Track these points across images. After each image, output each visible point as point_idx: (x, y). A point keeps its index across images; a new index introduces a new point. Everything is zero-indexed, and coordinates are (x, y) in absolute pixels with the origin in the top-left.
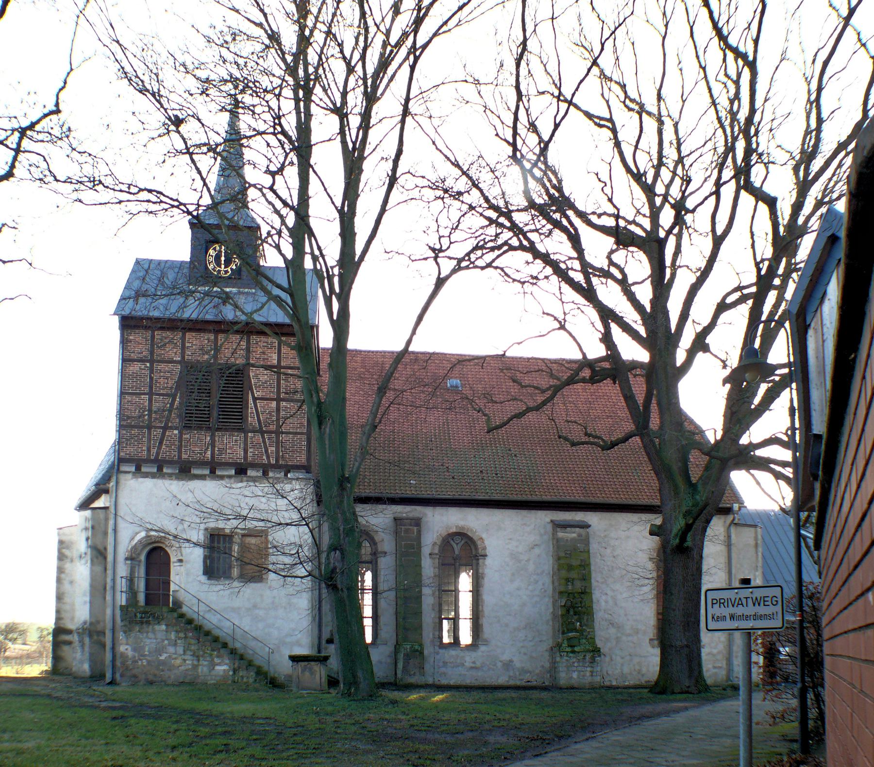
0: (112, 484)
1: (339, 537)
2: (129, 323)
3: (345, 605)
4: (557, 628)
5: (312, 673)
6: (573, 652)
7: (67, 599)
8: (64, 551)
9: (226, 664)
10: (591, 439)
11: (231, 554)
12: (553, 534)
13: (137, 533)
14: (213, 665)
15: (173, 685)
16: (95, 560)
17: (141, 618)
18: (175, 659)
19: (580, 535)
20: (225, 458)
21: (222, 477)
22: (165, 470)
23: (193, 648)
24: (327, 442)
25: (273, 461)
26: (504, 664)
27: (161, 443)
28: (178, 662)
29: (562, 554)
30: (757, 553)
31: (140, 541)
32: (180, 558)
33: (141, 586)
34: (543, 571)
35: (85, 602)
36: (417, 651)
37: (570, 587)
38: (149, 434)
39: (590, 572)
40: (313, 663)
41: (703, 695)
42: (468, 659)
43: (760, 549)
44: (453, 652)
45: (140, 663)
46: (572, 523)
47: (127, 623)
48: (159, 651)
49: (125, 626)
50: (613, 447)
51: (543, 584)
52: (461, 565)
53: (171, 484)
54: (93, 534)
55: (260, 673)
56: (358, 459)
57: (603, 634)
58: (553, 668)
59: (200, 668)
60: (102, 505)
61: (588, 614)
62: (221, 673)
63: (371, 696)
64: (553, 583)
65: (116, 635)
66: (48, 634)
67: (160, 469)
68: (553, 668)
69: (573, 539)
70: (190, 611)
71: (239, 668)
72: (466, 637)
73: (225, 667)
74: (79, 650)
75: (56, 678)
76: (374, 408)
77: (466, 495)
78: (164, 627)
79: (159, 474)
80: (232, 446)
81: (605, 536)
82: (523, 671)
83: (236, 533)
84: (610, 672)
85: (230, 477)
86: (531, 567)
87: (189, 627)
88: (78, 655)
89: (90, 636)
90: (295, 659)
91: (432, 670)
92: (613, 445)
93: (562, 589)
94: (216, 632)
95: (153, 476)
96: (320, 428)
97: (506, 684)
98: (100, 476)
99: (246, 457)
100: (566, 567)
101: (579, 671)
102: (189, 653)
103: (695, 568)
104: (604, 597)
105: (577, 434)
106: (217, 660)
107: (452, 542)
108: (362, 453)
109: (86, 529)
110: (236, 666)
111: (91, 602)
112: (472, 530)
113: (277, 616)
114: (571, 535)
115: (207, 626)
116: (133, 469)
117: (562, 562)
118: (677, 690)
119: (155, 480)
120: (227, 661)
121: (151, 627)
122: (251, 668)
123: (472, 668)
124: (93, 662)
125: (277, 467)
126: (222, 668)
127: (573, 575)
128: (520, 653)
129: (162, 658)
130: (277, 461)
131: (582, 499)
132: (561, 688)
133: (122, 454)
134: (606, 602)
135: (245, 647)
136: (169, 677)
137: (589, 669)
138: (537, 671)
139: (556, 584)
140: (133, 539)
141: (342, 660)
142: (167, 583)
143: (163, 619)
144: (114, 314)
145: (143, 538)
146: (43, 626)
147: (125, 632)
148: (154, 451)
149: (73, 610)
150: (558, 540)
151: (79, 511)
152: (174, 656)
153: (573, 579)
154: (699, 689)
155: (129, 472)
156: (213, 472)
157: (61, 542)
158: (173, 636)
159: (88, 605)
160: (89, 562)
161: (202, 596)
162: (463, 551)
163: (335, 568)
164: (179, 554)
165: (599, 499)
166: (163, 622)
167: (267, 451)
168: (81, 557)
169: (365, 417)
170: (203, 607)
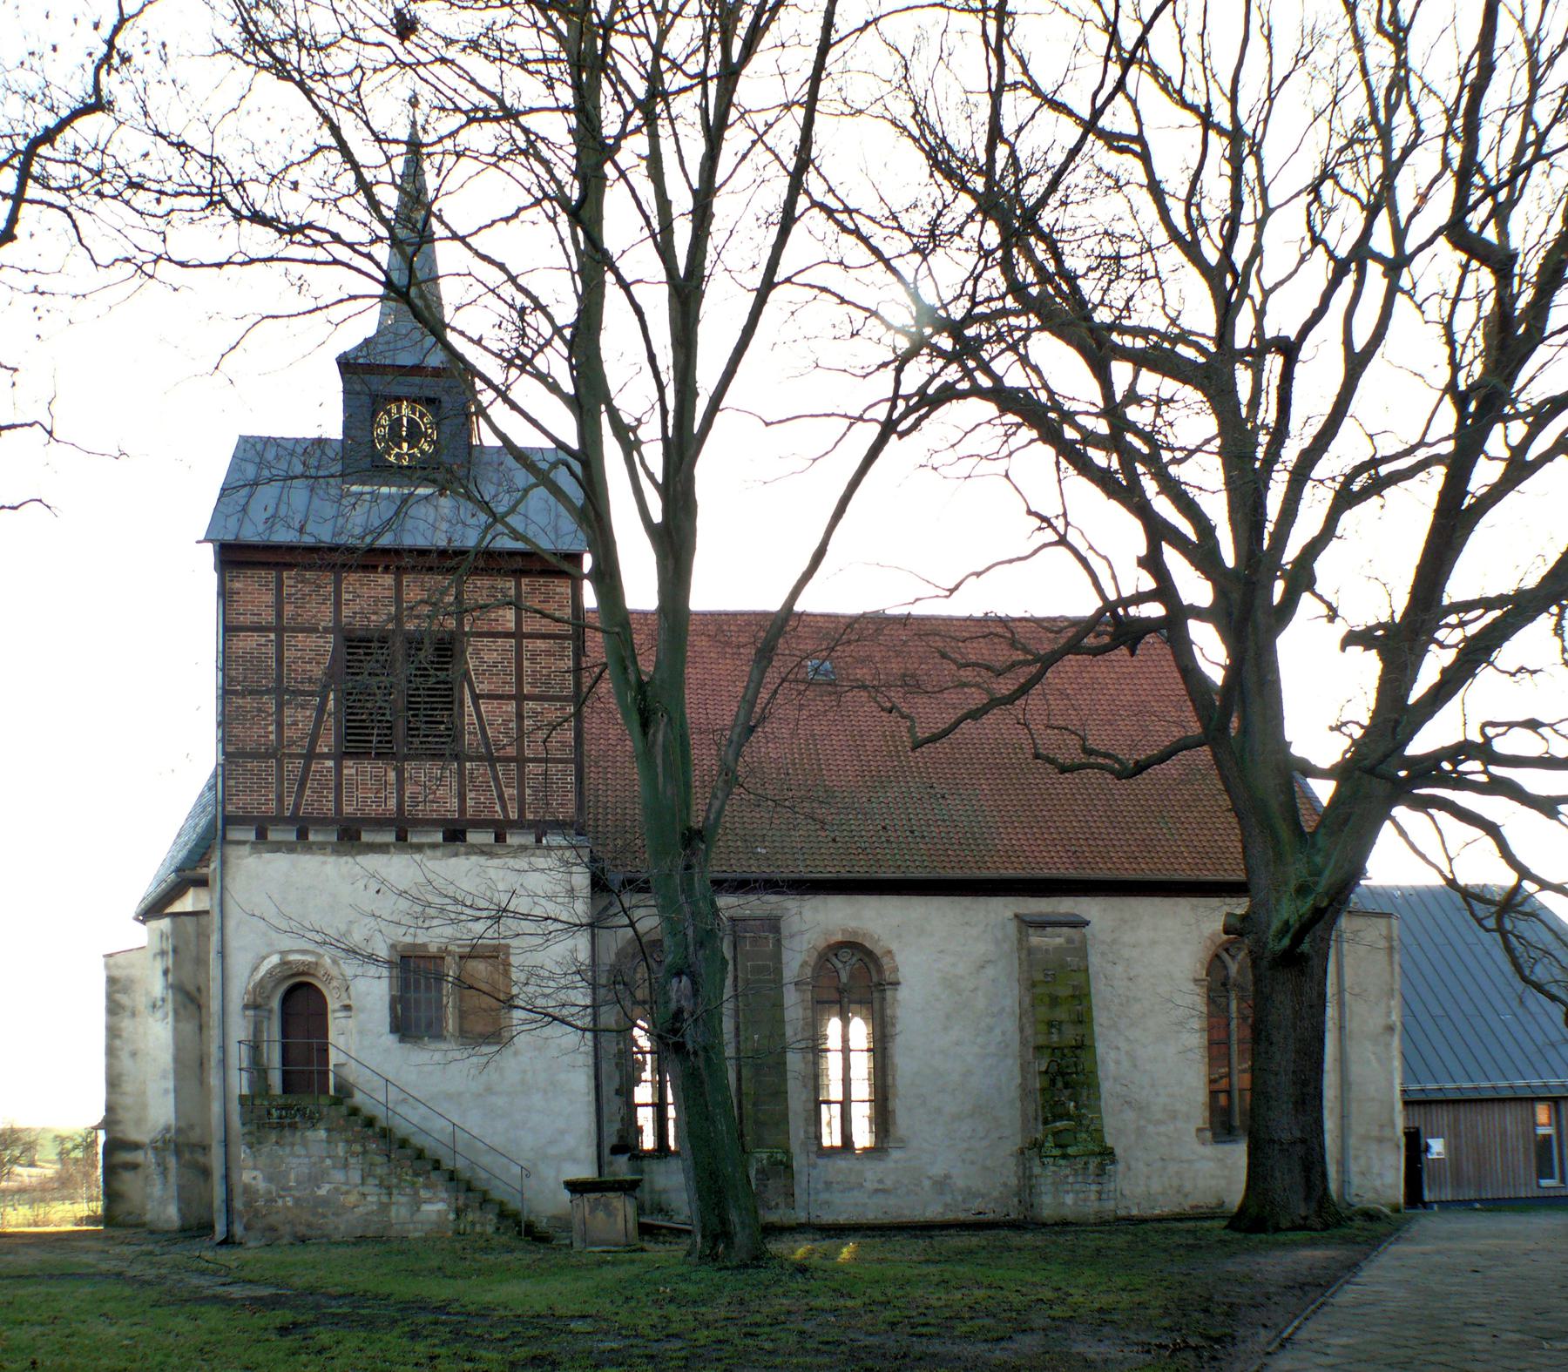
0: (214, 865)
1: (687, 948)
2: (233, 557)
3: (702, 1083)
4: (1031, 1113)
5: (610, 1213)
6: (1065, 1156)
7: (128, 1087)
8: (118, 996)
9: (443, 1200)
10: (1091, 759)
11: (437, 992)
12: (1020, 941)
13: (264, 958)
14: (417, 1203)
15: (346, 1243)
16: (182, 1011)
17: (280, 1117)
18: (347, 1193)
19: (1070, 941)
20: (422, 811)
21: (419, 848)
22: (312, 837)
23: (379, 1171)
24: (659, 761)
25: (513, 815)
26: (936, 1183)
27: (302, 785)
28: (352, 1198)
29: (1039, 976)
30: (1391, 963)
31: (270, 972)
32: (347, 1002)
33: (273, 1056)
34: (1003, 1009)
35: (166, 1091)
36: (781, 1162)
37: (1055, 1038)
38: (280, 767)
39: (1090, 1008)
40: (610, 1195)
41: (1334, 1231)
42: (869, 1175)
43: (1397, 957)
44: (842, 1163)
45: (280, 1202)
46: (1053, 919)
47: (254, 1128)
48: (315, 1179)
49: (250, 1133)
50: (1140, 772)
51: (1003, 1033)
52: (850, 1002)
53: (324, 863)
54: (175, 963)
55: (507, 1216)
56: (719, 794)
57: (1116, 1124)
58: (1027, 1186)
59: (394, 1209)
60: (189, 909)
61: (1089, 1086)
62: (434, 1217)
63: (756, 1258)
64: (1022, 1030)
65: (233, 1149)
66: (76, 1147)
67: (302, 835)
68: (1027, 1186)
69: (1057, 949)
70: (369, 1101)
71: (467, 1206)
72: (863, 1137)
73: (441, 1206)
74: (157, 1180)
75: (117, 1233)
76: (750, 693)
77: (860, 871)
78: (322, 1134)
79: (301, 842)
80: (434, 787)
81: (1114, 942)
82: (970, 1194)
83: (450, 953)
84: (1126, 1192)
85: (434, 846)
86: (981, 1002)
87: (370, 1132)
88: (157, 1190)
89: (178, 1153)
90: (575, 1187)
91: (805, 1198)
92: (1141, 767)
93: (1041, 1040)
94: (418, 1141)
95: (290, 848)
96: (645, 734)
97: (939, 1218)
98: (184, 853)
99: (462, 810)
100: (1047, 1000)
101: (1077, 1193)
102: (371, 1181)
103: (1315, 994)
104: (1113, 1054)
105: (1070, 752)
106: (423, 1194)
107: (834, 960)
108: (726, 782)
109: (163, 953)
110: (461, 1202)
111: (176, 1090)
112: (871, 937)
113: (529, 1107)
114: (1053, 940)
115: (402, 1128)
116: (252, 836)
117: (1039, 990)
118: (1284, 1223)
119: (294, 856)
120: (444, 1195)
121: (299, 1134)
122: (489, 1207)
123: (877, 1191)
124: (184, 1201)
125: (520, 825)
126: (436, 1207)
127: (1061, 1014)
128: (963, 1161)
129: (322, 1192)
130: (521, 812)
131: (1072, 874)
132: (1045, 1225)
133: (229, 808)
134: (1118, 1063)
135: (473, 1164)
136: (336, 1228)
137: (1094, 1187)
138: (996, 1194)
139: (1029, 1031)
140: (256, 969)
141: (699, 1191)
142: (324, 1051)
143: (319, 1120)
144: (206, 540)
145: (274, 967)
146: (64, 1133)
147: (250, 1146)
148: (290, 801)
149: (144, 1106)
150: (1030, 952)
151: (143, 922)
152: (344, 1188)
153: (1061, 1023)
154: (1331, 1218)
155: (243, 843)
156: (401, 837)
157: (112, 981)
158: (341, 1150)
159: (172, 1095)
160: (171, 1014)
161: (390, 1071)
162: (857, 979)
163: (680, 1011)
164: (344, 995)
165: (1103, 873)
166: (322, 1125)
167: (501, 797)
168: (154, 1006)
169: (726, 713)
170: (393, 1094)
